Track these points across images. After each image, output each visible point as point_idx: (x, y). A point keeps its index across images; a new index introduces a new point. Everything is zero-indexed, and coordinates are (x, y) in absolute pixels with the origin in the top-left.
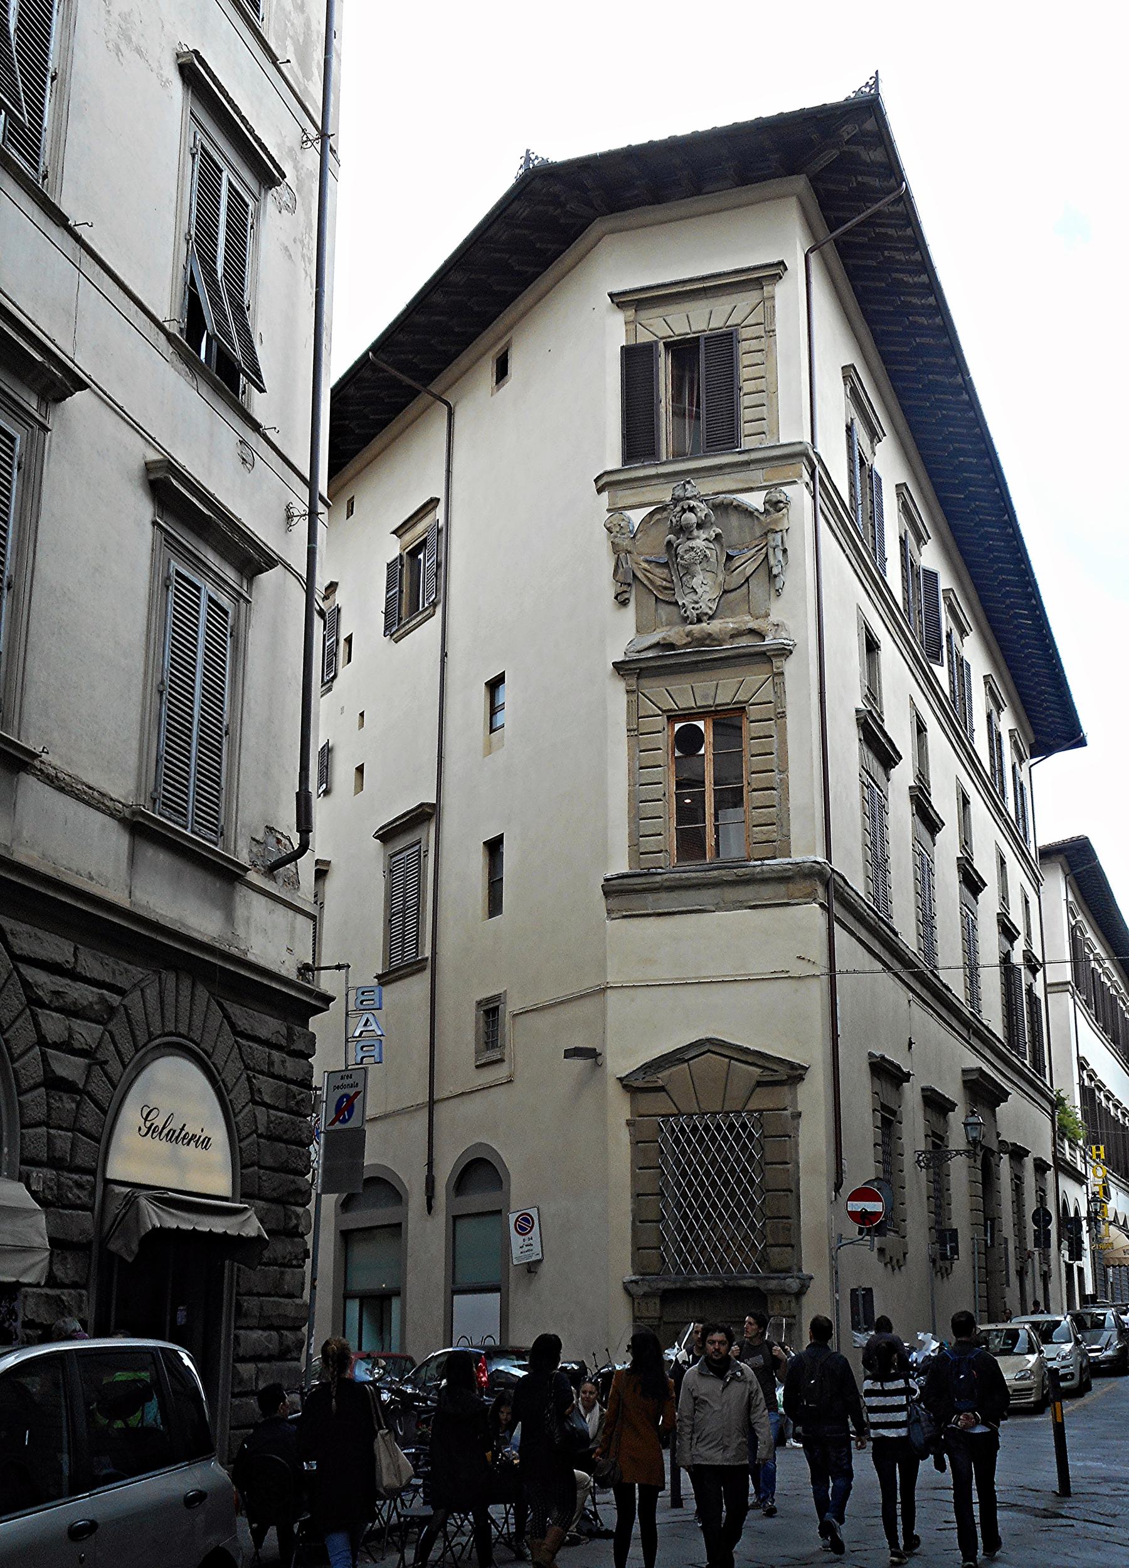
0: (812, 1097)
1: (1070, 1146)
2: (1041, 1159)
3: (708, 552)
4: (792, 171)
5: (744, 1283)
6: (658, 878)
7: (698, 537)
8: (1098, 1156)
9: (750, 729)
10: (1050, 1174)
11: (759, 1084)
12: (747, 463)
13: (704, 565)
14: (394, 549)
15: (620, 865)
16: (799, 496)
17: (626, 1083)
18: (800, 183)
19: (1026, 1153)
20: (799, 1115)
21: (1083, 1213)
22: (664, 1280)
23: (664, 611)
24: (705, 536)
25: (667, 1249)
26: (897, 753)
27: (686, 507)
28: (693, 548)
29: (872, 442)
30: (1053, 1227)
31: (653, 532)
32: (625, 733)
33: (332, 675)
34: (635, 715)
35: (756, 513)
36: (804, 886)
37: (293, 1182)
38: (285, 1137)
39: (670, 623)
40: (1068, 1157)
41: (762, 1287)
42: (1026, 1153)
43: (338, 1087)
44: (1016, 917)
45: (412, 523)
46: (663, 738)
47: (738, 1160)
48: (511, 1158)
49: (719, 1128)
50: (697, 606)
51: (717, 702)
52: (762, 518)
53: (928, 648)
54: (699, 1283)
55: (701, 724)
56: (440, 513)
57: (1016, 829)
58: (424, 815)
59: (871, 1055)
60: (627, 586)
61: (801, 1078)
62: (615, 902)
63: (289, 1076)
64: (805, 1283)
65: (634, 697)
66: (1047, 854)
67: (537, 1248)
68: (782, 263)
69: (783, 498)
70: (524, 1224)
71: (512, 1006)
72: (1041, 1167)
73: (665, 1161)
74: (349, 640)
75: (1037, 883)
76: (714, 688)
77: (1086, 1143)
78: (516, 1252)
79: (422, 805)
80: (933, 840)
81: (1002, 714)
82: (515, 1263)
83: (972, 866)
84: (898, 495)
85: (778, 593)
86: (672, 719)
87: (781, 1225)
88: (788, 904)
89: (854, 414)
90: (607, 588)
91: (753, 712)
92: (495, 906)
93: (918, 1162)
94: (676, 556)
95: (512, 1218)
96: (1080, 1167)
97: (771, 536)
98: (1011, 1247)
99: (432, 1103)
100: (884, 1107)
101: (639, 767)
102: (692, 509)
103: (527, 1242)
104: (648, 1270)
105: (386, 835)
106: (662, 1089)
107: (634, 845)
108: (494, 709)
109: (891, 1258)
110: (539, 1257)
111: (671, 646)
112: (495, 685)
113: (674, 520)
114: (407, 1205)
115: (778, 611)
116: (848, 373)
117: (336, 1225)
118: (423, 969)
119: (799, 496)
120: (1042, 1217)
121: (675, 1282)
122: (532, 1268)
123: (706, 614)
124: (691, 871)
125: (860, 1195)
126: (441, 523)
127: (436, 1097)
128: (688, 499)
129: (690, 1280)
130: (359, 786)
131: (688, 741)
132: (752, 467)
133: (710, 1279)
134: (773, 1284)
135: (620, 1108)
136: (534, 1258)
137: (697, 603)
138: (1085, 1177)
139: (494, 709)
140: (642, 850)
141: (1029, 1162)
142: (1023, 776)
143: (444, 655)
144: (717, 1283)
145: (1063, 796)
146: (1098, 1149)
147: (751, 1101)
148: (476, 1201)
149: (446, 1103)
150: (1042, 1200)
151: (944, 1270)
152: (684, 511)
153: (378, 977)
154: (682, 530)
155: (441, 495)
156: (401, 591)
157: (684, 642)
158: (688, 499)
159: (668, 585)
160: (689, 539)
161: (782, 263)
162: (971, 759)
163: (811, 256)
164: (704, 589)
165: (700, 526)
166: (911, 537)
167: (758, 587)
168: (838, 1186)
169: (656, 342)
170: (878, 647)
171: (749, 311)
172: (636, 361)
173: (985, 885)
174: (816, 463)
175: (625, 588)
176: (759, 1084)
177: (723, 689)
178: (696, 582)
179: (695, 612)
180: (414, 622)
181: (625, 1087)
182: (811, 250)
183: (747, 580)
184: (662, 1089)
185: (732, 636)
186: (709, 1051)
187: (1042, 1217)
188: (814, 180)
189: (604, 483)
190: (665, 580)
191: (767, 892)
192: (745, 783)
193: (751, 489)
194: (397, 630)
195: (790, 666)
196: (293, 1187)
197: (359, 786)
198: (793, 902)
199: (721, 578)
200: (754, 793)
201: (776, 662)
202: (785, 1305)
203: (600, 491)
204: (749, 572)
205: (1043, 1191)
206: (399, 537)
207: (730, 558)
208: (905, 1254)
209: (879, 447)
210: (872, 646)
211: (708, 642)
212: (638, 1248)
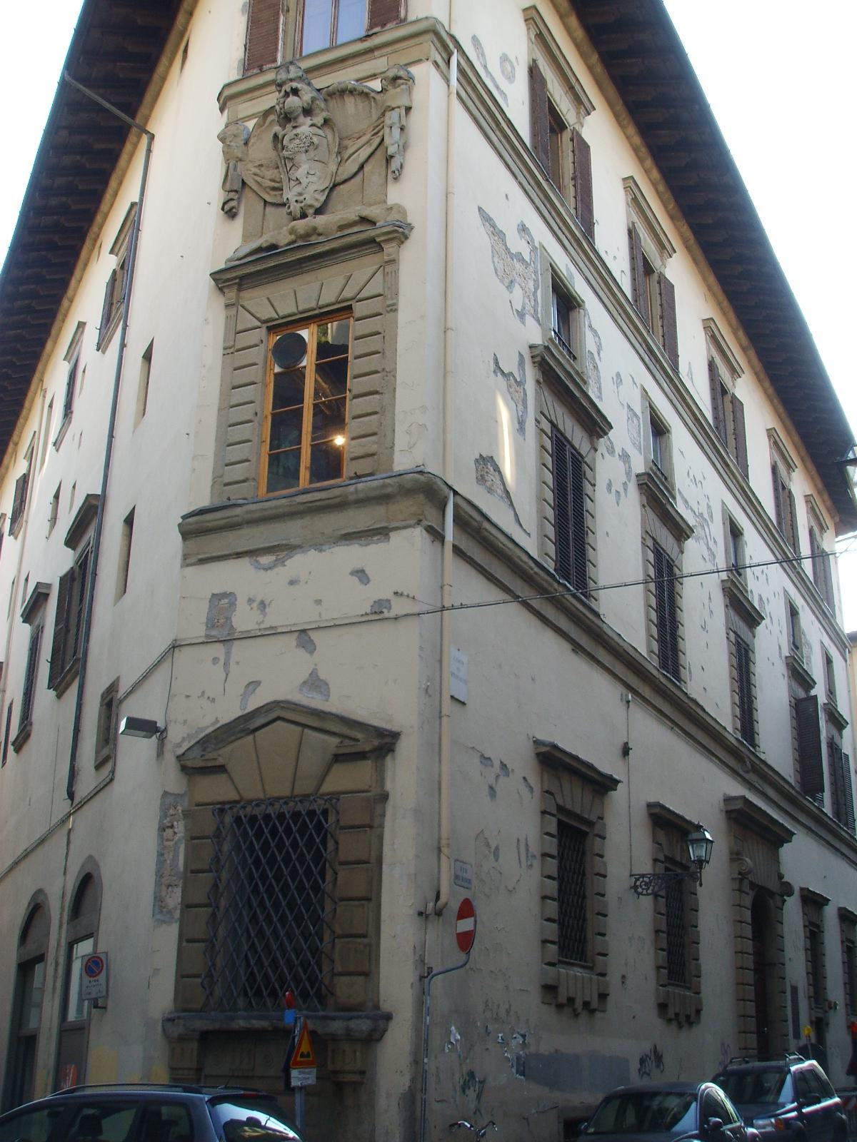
3: (315, 140)
6: (238, 511)
7: (304, 124)
11: (338, 758)
12: (371, 50)
13: (312, 153)
19: (826, 901)
27: (288, 90)
28: (296, 135)
35: (373, 94)
36: (406, 507)
42: (826, 901)
47: (302, 859)
50: (301, 198)
51: (320, 303)
52: (378, 97)
55: (305, 333)
62: (193, 543)
65: (233, 311)
83: (836, 710)
86: (271, 330)
89: (813, 524)
97: (388, 114)
106: (221, 769)
111: (273, 247)
123: (311, 206)
124: (280, 502)
128: (291, 80)
131: (289, 350)
132: (377, 53)
137: (300, 194)
147: (328, 779)
151: (682, 1018)
152: (287, 95)
154: (287, 118)
155: (137, 200)
157: (286, 241)
158: (291, 80)
159: (276, 185)
160: (295, 127)
164: (309, 181)
166: (816, 529)
174: (451, 46)
175: (232, 195)
176: (338, 758)
177: (322, 287)
178: (300, 173)
179: (299, 205)
183: (362, 167)
184: (221, 769)
186: (278, 718)
201: (389, 249)
204: (362, 159)
211: (314, 239)
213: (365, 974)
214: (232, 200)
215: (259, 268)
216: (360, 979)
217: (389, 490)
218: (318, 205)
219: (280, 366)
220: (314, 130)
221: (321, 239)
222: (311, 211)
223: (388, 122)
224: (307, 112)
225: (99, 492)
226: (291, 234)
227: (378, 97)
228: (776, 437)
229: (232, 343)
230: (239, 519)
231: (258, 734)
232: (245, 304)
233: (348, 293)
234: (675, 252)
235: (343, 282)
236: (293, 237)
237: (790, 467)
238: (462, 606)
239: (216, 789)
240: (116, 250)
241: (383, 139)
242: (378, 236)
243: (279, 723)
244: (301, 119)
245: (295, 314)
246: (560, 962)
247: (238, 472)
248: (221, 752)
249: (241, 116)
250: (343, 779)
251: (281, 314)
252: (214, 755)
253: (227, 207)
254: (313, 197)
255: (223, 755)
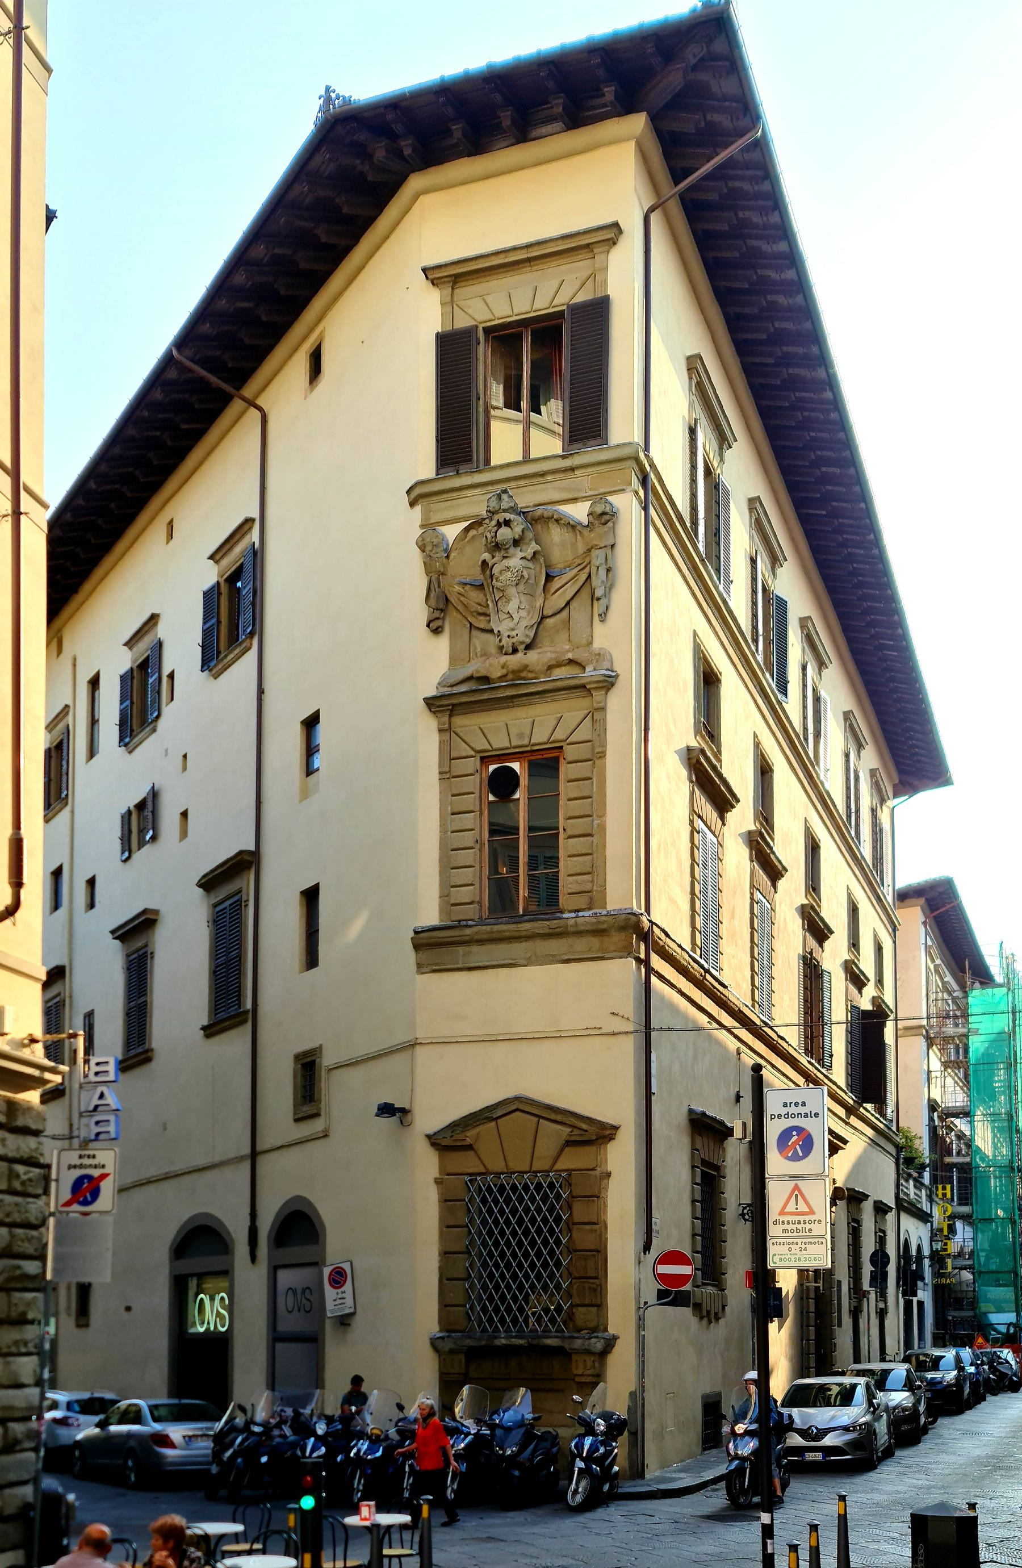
0: (621, 1158)
1: (915, 1186)
2: (881, 1202)
4: (626, 107)
5: (549, 1342)
6: (468, 931)
8: (944, 1195)
9: (566, 771)
10: (891, 1217)
11: (568, 1143)
12: (572, 469)
13: (521, 587)
14: (210, 575)
15: (431, 917)
16: (627, 505)
17: (434, 1140)
18: (638, 123)
20: (609, 1175)
21: (926, 1252)
22: (470, 1338)
23: (480, 640)
24: (522, 554)
25: (472, 1308)
26: (734, 796)
27: (502, 520)
29: (721, 448)
30: (892, 1269)
31: (469, 550)
32: (437, 776)
33: (156, 714)
34: (448, 758)
36: (616, 939)
37: (19, 1267)
38: (7, 1220)
39: (485, 654)
40: (912, 1196)
41: (566, 1346)
43: (75, 1167)
44: (867, 965)
45: (228, 546)
46: (474, 783)
48: (328, 1211)
49: (526, 1188)
50: (514, 633)
51: (533, 741)
53: (770, 678)
54: (504, 1341)
55: (516, 766)
56: (255, 536)
57: (871, 872)
58: (244, 864)
59: (691, 1111)
60: (441, 610)
61: (611, 1138)
62: (425, 955)
63: (10, 1155)
64: (610, 1343)
65: (446, 737)
66: (903, 896)
67: (349, 1301)
68: (616, 225)
69: (608, 509)
70: (338, 1278)
71: (328, 1060)
72: (880, 1209)
73: (472, 1220)
74: (171, 676)
75: (894, 929)
76: (529, 726)
77: (934, 1180)
78: (330, 1305)
79: (241, 852)
80: (774, 886)
81: (863, 753)
82: (329, 1315)
83: (818, 914)
84: (751, 510)
85: (603, 617)
87: (587, 1286)
88: (602, 958)
89: (699, 413)
90: (421, 613)
91: (570, 752)
92: (311, 960)
93: (743, 1215)
94: (492, 576)
95: (327, 1271)
96: (925, 1206)
97: (595, 553)
98: (845, 1288)
99: (254, 1155)
100: (704, 1163)
101: (450, 813)
102: (507, 523)
103: (340, 1296)
104: (454, 1327)
105: (209, 883)
106: (470, 1147)
107: (444, 896)
108: (311, 750)
109: (708, 1312)
110: (352, 1310)
111: (485, 679)
112: (311, 723)
113: (489, 536)
114: (233, 1254)
115: (603, 637)
116: (694, 365)
117: (171, 1270)
118: (245, 1021)
119: (627, 505)
120: (880, 1258)
121: (480, 1340)
122: (344, 1321)
123: (522, 643)
125: (672, 1257)
126: (257, 545)
127: (259, 1147)
129: (496, 1338)
130: (184, 834)
131: (503, 784)
133: (515, 1337)
134: (578, 1344)
135: (427, 1164)
136: (347, 1311)
137: (513, 630)
138: (931, 1215)
139: (311, 750)
140: (453, 901)
141: (868, 1206)
142: (884, 817)
143: (261, 691)
144: (521, 1342)
145: (922, 837)
146: (944, 1188)
148: (295, 1253)
149: (275, 1155)
150: (881, 1241)
152: (499, 525)
153: (204, 1028)
155: (255, 514)
156: (219, 622)
157: (499, 674)
158: (504, 511)
160: (505, 557)
161: (616, 225)
162: (823, 800)
163: (653, 217)
164: (515, 617)
165: (516, 543)
167: (579, 611)
168: (647, 1247)
169: (477, 327)
170: (719, 681)
171: (578, 286)
172: (453, 351)
173: (832, 932)
174: (648, 468)
175: (437, 614)
176: (568, 1143)
178: (512, 607)
180: (232, 656)
181: (433, 1145)
182: (652, 209)
184: (470, 1147)
185: (550, 668)
187: (880, 1258)
188: (654, 119)
189: (417, 494)
190: (480, 605)
191: (580, 945)
192: (561, 830)
193: (574, 500)
194: (215, 666)
195: (614, 701)
196: (18, 1272)
197: (184, 834)
198: (607, 955)
199: (539, 602)
200: (570, 840)
201: (598, 695)
202: (589, 1363)
203: (412, 504)
205: (884, 1232)
206: (217, 562)
207: (549, 578)
208: (724, 1307)
209: (728, 454)
210: (708, 681)
211: (523, 674)
212: (444, 1305)
213: (598, 1306)
214: (438, 618)
215: (472, 699)
216: (594, 1309)
217: (604, 926)
218: (528, 641)
219: (494, 795)
220: (524, 563)
221: (530, 675)
222: (522, 647)
223: (596, 562)
224: (516, 543)
225: (252, 848)
226: (503, 667)
227: (586, 532)
228: (760, 511)
229: (447, 769)
230: (467, 938)
231: (499, 1121)
232: (458, 730)
233: (559, 735)
234: (736, 441)
235: (554, 723)
236: (504, 671)
237: (775, 561)
238: (669, 1029)
239: (468, 1163)
240: (217, 557)
241: (589, 576)
242: (590, 683)
243: (517, 1113)
244: (512, 550)
245: (507, 748)
246: (703, 1284)
247: (465, 894)
248: (468, 1134)
249: (433, 521)
250: (570, 1160)
251: (494, 747)
252: (461, 1137)
253: (433, 625)
254: (522, 634)
255: (470, 1136)
